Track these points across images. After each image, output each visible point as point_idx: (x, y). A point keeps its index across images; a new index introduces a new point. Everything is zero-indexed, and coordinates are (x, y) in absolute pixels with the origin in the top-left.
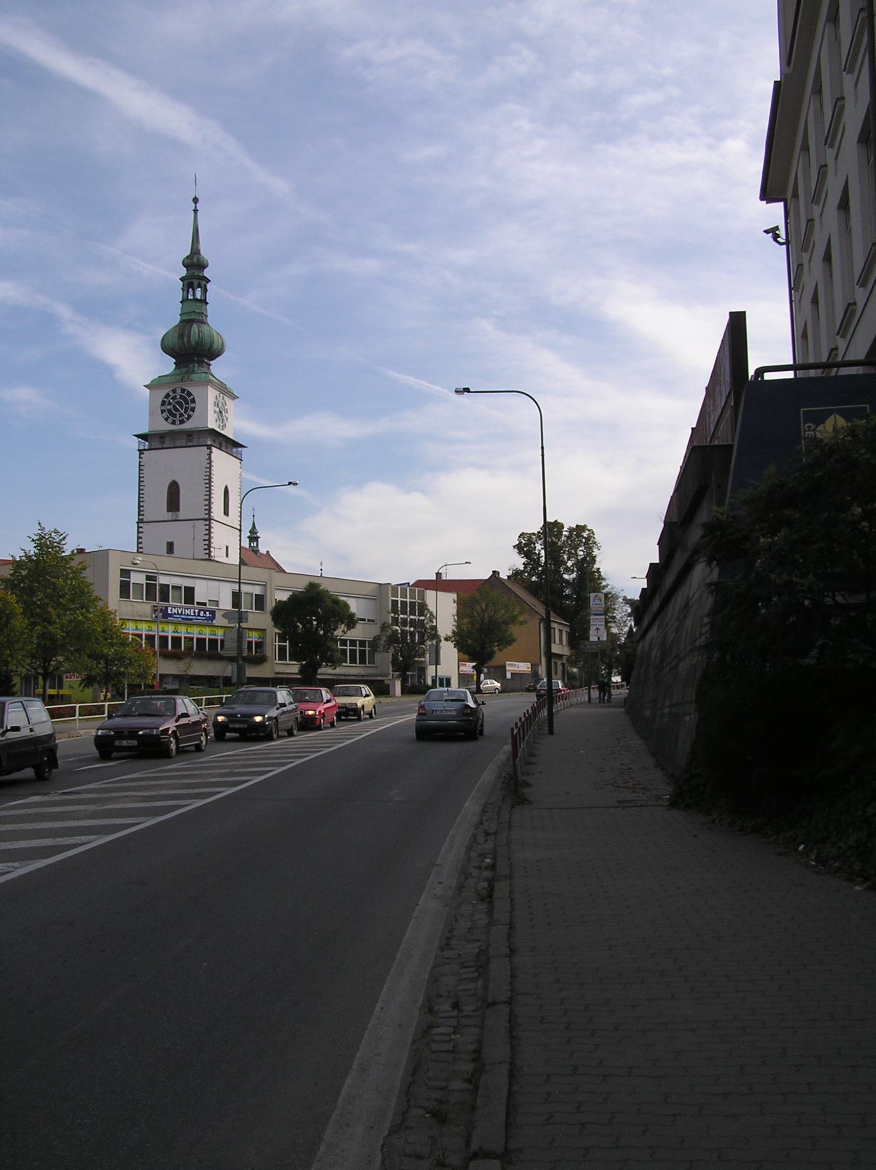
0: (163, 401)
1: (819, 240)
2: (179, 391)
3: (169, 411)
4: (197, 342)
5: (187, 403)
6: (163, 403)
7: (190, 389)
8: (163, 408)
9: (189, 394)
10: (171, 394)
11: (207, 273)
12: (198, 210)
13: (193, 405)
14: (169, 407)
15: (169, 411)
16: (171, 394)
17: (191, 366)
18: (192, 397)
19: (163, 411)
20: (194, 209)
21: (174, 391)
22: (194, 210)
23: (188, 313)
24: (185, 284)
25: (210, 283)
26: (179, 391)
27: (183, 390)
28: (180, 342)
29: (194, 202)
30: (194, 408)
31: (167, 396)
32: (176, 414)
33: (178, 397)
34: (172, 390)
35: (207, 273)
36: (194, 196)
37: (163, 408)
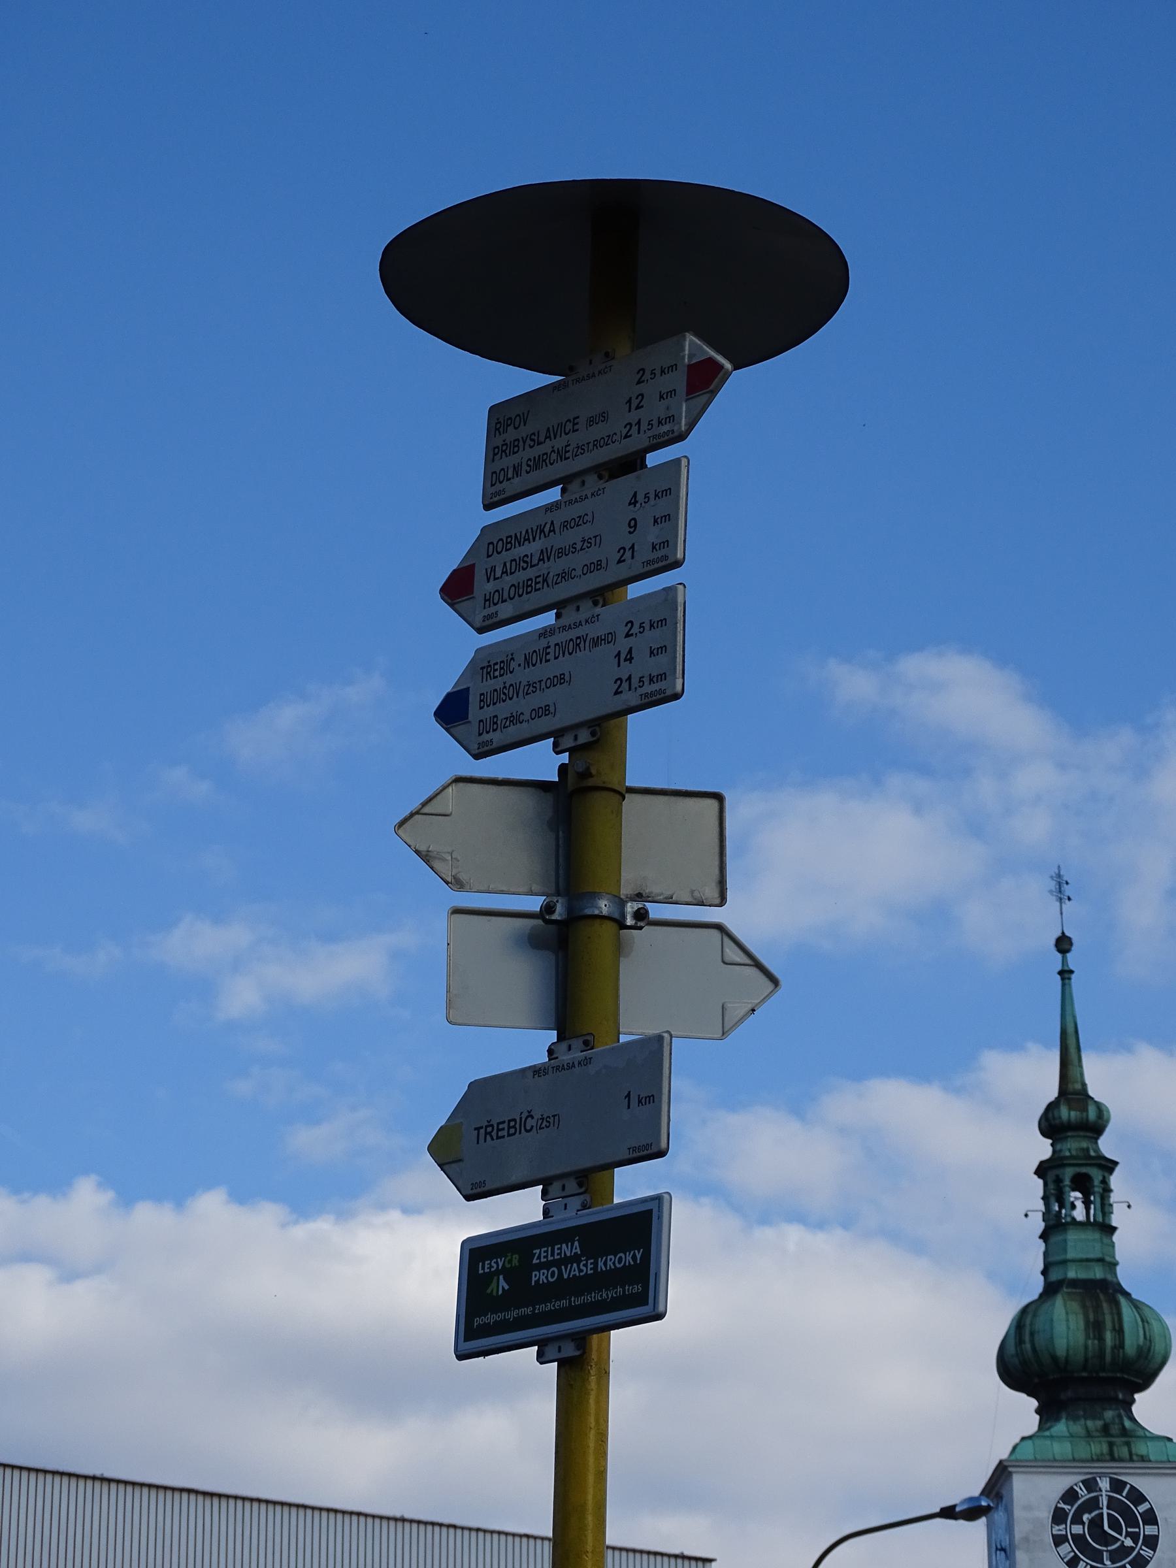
0: (1057, 1510)
1: (542, 687)
2: (1104, 1484)
3: (1079, 1540)
4: (1140, 1349)
5: (1132, 1521)
6: (1059, 1517)
7: (1142, 1484)
8: (1059, 1530)
9: (1138, 1497)
10: (1082, 1492)
11: (1107, 1145)
12: (1072, 972)
13: (1150, 1530)
14: (1077, 1529)
15: (1079, 1540)
16: (1082, 1492)
17: (1109, 1414)
18: (1062, 1505)
19: (1059, 1540)
20: (1059, 968)
21: (1090, 1484)
22: (1061, 973)
23: (1081, 1261)
24: (1050, 1180)
25: (1118, 1170)
26: (1104, 1484)
27: (1117, 1485)
28: (1092, 1344)
29: (1060, 951)
30: (1156, 1538)
31: (1070, 1496)
32: (1101, 1552)
33: (1077, 1529)
34: (1083, 1482)
35: (1107, 1145)
36: (1059, 934)
37: (1059, 1530)
